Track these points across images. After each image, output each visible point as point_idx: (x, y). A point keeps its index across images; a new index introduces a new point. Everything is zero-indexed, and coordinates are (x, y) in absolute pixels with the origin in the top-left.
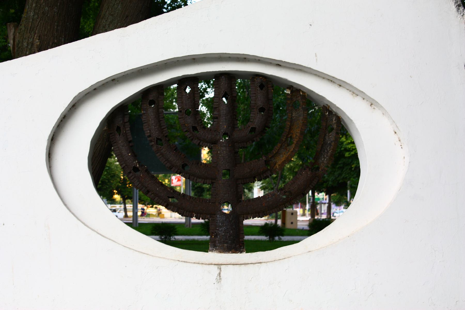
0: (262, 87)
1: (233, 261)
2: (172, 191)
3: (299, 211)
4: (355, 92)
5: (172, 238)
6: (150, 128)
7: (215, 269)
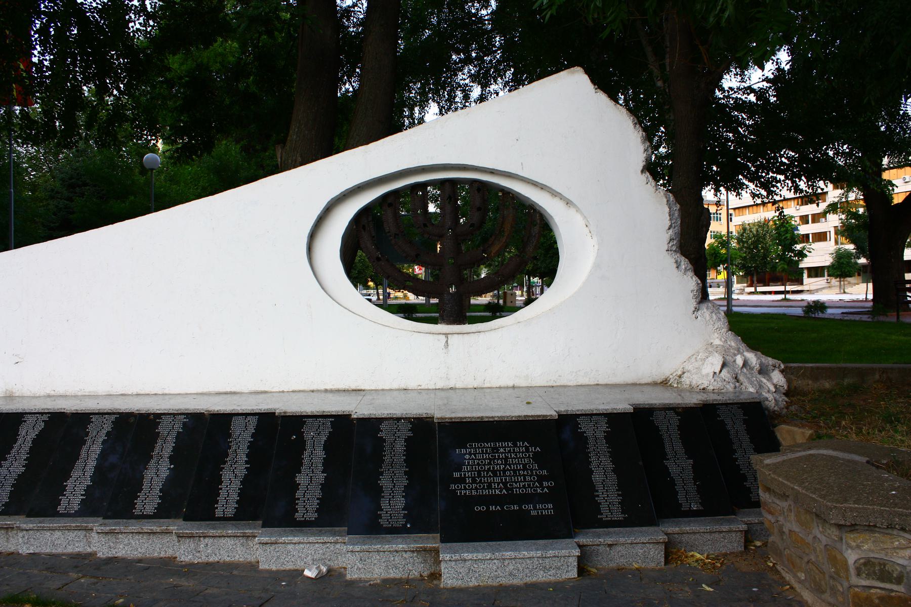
0: (479, 190)
1: (458, 331)
2: (415, 278)
3: (518, 293)
4: (554, 193)
5: (414, 316)
6: (390, 226)
7: (443, 338)
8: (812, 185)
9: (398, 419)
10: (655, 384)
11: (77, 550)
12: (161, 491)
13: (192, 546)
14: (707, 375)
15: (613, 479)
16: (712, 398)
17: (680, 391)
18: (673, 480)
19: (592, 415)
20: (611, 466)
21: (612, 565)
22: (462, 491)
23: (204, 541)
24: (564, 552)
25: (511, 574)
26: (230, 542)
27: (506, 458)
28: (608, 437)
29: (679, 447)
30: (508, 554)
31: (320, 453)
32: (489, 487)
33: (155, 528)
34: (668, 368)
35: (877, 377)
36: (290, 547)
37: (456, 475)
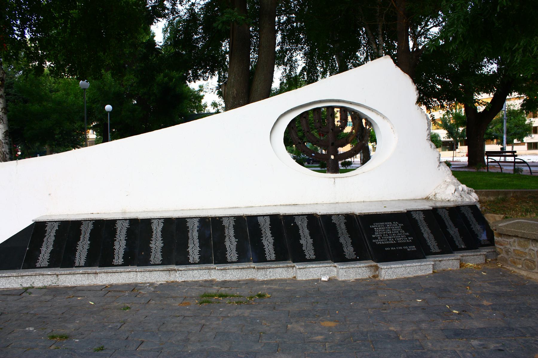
8: (450, 104)
9: (338, 215)
10: (423, 199)
11: (205, 278)
12: (236, 251)
13: (264, 273)
14: (449, 194)
15: (431, 236)
16: (457, 204)
17: (436, 201)
18: (452, 236)
19: (416, 211)
20: (429, 231)
21: (441, 269)
22: (379, 242)
23: (269, 270)
24: (428, 263)
25: (408, 273)
26: (280, 270)
27: (391, 229)
28: (425, 220)
29: (451, 223)
30: (408, 265)
31: (307, 232)
32: (388, 240)
33: (244, 266)
34: (428, 192)
35: (512, 195)
36: (311, 269)
37: (373, 236)
